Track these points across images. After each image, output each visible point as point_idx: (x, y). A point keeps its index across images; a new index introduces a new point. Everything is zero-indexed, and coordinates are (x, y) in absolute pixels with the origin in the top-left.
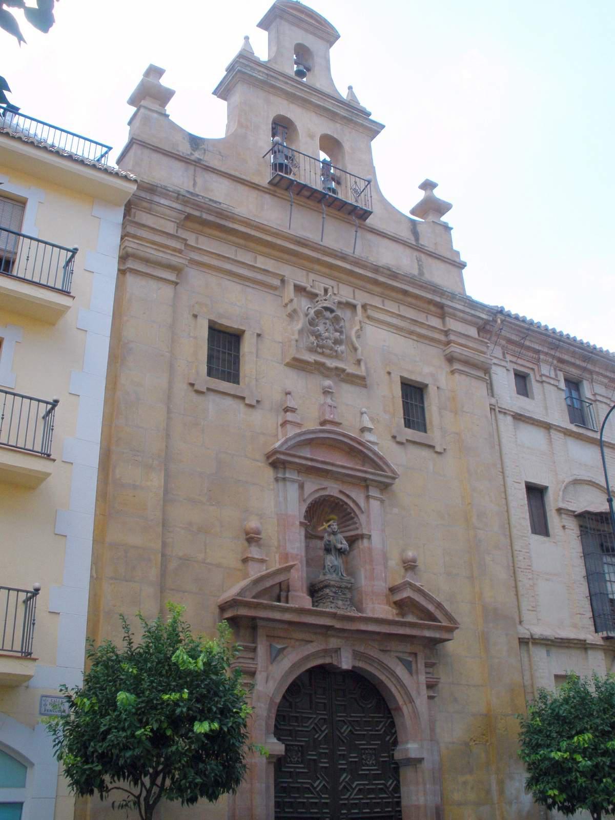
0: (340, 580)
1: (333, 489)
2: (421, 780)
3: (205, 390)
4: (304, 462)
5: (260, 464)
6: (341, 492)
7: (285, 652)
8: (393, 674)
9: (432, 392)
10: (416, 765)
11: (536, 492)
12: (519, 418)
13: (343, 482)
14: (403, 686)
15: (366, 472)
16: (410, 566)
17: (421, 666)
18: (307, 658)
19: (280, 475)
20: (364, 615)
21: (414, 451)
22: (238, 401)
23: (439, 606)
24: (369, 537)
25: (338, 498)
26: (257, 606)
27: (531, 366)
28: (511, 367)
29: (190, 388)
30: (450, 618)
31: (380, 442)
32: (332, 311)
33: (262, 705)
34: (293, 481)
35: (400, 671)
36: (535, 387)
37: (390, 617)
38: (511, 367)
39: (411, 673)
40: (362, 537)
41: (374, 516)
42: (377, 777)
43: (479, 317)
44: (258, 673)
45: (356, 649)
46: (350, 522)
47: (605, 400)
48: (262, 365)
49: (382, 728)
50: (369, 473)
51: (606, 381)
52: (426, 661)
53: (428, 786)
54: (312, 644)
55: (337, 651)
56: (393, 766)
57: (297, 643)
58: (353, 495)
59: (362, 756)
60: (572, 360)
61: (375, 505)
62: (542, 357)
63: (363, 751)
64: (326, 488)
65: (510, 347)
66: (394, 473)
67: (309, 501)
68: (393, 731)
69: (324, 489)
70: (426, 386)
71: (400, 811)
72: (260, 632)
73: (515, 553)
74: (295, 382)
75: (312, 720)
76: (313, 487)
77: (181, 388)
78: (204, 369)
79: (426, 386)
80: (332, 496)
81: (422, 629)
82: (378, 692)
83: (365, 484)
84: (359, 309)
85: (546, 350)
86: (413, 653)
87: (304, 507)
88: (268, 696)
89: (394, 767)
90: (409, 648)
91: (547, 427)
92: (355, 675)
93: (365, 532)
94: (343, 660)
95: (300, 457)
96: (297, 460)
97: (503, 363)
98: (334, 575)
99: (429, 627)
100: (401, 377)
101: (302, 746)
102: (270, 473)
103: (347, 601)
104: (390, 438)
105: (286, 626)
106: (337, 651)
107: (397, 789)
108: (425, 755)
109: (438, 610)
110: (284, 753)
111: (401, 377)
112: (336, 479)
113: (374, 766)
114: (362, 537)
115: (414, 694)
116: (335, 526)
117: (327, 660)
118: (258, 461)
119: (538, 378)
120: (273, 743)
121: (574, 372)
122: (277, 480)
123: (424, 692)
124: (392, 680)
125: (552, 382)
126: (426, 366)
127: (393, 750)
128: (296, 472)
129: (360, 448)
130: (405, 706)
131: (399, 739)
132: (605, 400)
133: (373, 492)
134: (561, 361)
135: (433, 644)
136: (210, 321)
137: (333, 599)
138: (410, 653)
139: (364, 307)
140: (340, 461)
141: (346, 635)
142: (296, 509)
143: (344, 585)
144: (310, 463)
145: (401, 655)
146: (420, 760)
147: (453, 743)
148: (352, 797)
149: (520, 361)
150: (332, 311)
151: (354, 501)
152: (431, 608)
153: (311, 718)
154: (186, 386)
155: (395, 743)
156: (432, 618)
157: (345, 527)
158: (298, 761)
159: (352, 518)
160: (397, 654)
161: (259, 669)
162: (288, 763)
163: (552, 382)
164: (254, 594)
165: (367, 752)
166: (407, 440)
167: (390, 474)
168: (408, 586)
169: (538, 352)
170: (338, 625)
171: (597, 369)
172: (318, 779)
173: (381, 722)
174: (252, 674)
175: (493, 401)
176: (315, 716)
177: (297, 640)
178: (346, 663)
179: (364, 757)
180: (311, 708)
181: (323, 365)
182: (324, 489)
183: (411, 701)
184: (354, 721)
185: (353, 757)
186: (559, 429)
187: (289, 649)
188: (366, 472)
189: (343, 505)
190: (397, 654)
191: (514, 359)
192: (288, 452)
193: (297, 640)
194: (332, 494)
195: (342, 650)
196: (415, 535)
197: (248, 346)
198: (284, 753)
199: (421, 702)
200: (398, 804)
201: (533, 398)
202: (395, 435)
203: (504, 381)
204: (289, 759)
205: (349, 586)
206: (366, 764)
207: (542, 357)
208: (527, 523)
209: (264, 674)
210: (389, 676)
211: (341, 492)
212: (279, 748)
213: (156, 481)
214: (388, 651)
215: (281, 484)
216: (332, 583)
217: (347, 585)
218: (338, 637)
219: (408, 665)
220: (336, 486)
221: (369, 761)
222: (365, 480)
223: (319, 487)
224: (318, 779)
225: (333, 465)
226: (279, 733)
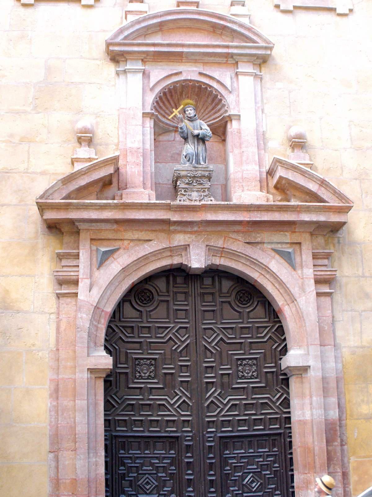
0: (193, 169)
1: (190, 72)
2: (307, 392)
4: (152, 49)
5: (98, 62)
6: (201, 74)
7: (115, 256)
8: (266, 269)
10: (301, 374)
13: (205, 63)
14: (281, 283)
15: (228, 47)
16: (298, 143)
17: (306, 256)
18: (145, 259)
19: (121, 69)
20: (231, 203)
23: (323, 183)
24: (238, 117)
25: (198, 82)
26: (67, 207)
30: (340, 196)
33: (84, 316)
34: (135, 71)
35: (276, 265)
37: (262, 202)
39: (293, 266)
40: (230, 118)
41: (241, 93)
42: (260, 390)
44: (80, 280)
45: (212, 244)
46: (219, 106)
49: (265, 335)
50: (235, 47)
52: (314, 251)
53: (314, 398)
54: (151, 243)
55: (186, 247)
56: (281, 377)
57: (132, 244)
58: (216, 75)
59: (238, 367)
61: (246, 83)
63: (239, 362)
64: (181, 73)
66: (267, 43)
67: (158, 89)
68: (283, 338)
69: (176, 74)
71: (290, 428)
72: (82, 235)
75: (169, 329)
76: (159, 73)
80: (190, 81)
82: (261, 293)
83: (230, 60)
86: (297, 243)
87: (151, 98)
88: (92, 305)
89: (283, 379)
90: (287, 237)
92: (214, 273)
93: (232, 112)
94: (193, 257)
96: (136, 49)
98: (188, 164)
99: (308, 210)
101: (155, 359)
102: (111, 68)
103: (204, 191)
104: (272, 7)
105: (115, 226)
106: (186, 247)
107: (286, 403)
108: (311, 363)
109: (323, 189)
110: (111, 367)
112: (196, 62)
113: (256, 378)
114: (230, 118)
115: (295, 291)
116: (189, 111)
117: (176, 261)
118: (97, 59)
120: (101, 356)
122: (118, 74)
123: (311, 287)
124: (267, 276)
127: (281, 359)
128: (140, 61)
129: (222, 22)
130: (287, 307)
131: (288, 347)
135: (335, 229)
137: (185, 191)
138: (292, 243)
141: (196, 229)
143: (199, 173)
144: (152, 49)
145: (279, 247)
146: (305, 369)
147: (363, 347)
148: (223, 413)
151: (218, 82)
152: (313, 187)
153: (167, 328)
155: (285, 351)
156: (315, 197)
157: (216, 113)
158: (149, 376)
159: (221, 100)
160: (273, 246)
161: (81, 276)
162: (138, 379)
164: (64, 195)
165: (244, 362)
166: (295, 7)
168: (278, 164)
170: (175, 217)
172: (177, 395)
173: (266, 327)
174: (76, 283)
176: (172, 325)
177: (132, 240)
178: (197, 261)
179: (240, 368)
180: (168, 317)
182: (176, 74)
183: (293, 300)
184: (224, 328)
185: (226, 369)
187: (121, 251)
188: (228, 47)
189: (206, 88)
190: (273, 246)
192: (126, 41)
193: (132, 240)
194: (189, 78)
195: (191, 247)
198: (111, 367)
200: (288, 420)
202: (278, 3)
204: (138, 374)
205: (207, 174)
206: (243, 376)
209: (88, 281)
210: (263, 273)
211: (201, 74)
214: (258, 243)
215: (122, 77)
216: (183, 173)
217: (203, 173)
218: (185, 232)
219: (287, 257)
220: (195, 69)
221: (248, 373)
222: (232, 55)
223: (170, 73)
224: (177, 395)
225: (183, 46)
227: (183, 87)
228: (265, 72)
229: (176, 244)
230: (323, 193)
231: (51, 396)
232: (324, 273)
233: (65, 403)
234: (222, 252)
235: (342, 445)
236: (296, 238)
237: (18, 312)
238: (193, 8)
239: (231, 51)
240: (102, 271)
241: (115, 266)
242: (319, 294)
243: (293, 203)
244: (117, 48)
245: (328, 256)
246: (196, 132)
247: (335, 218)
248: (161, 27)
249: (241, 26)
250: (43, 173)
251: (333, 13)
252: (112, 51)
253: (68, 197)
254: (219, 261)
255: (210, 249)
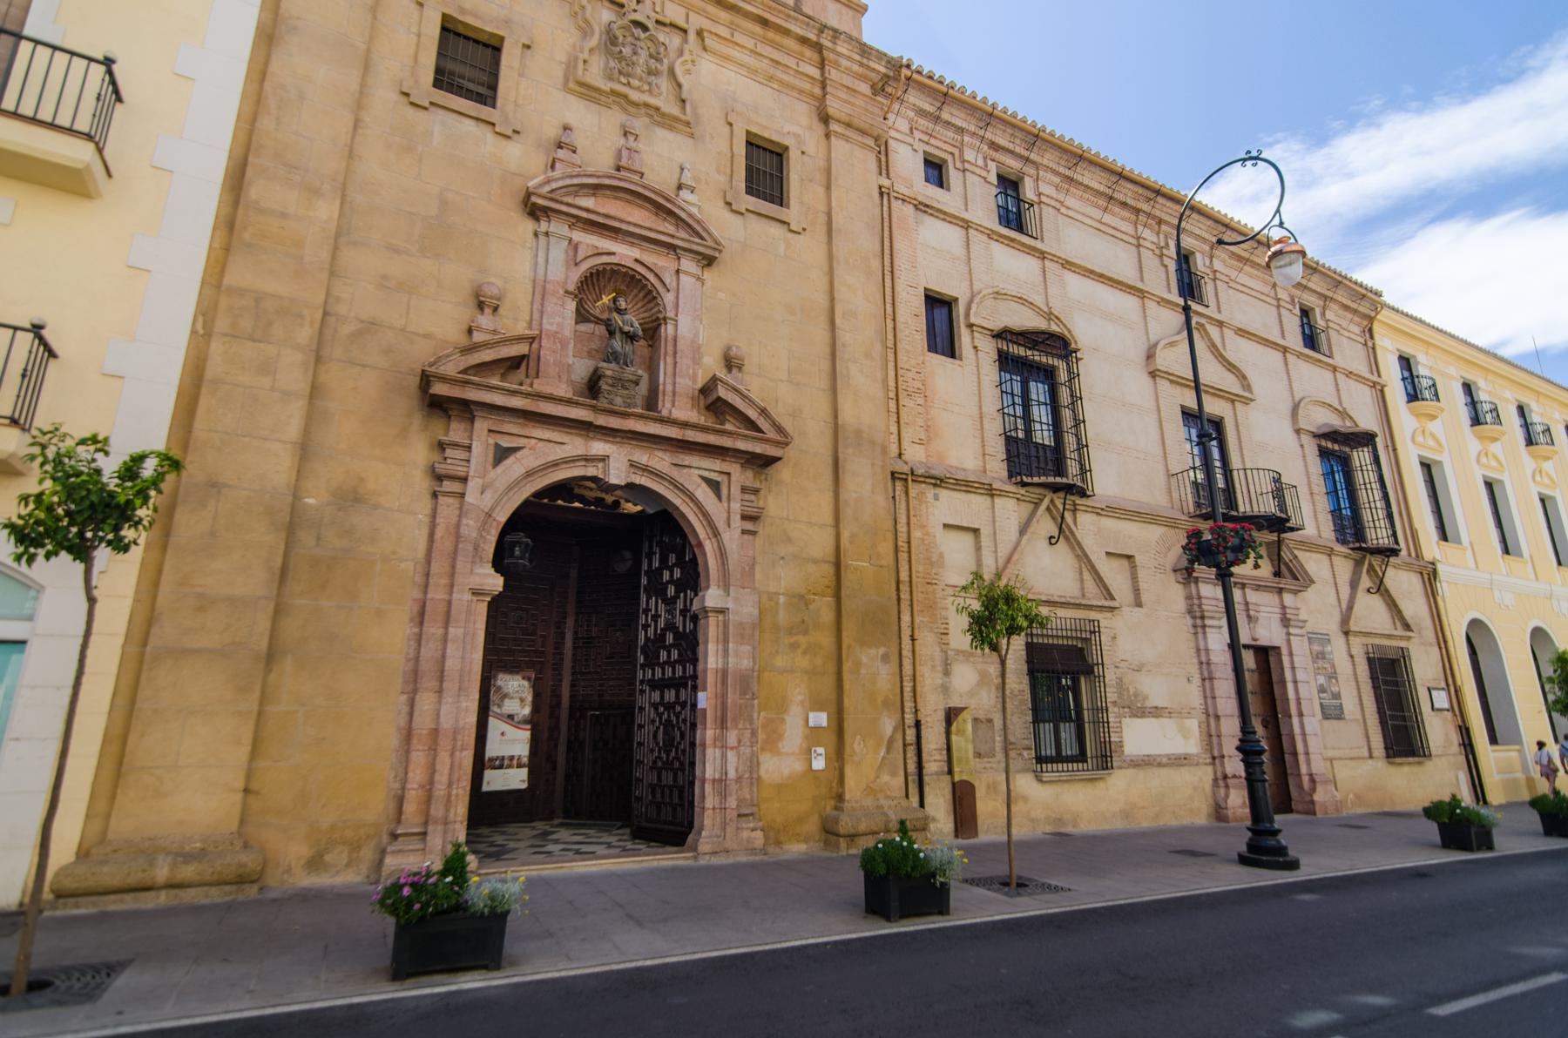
1: (625, 253)
3: (426, 104)
9: (794, 156)
11: (937, 304)
12: (923, 207)
21: (756, 225)
22: (483, 127)
23: (763, 412)
27: (950, 149)
28: (921, 147)
29: (404, 99)
30: (779, 429)
31: (702, 204)
32: (645, 28)
34: (561, 237)
36: (953, 176)
38: (921, 147)
43: (874, 70)
47: (1053, 203)
48: (532, 87)
50: (681, 237)
51: (1057, 180)
60: (1011, 146)
62: (966, 139)
65: (922, 122)
67: (584, 267)
70: (786, 148)
73: (900, 372)
74: (579, 114)
77: (384, 97)
78: (428, 75)
79: (786, 148)
81: (737, 433)
84: (692, 36)
85: (972, 128)
87: (576, 275)
91: (966, 225)
95: (568, 205)
97: (910, 140)
100: (748, 132)
111: (748, 132)
115: (721, 525)
117: (591, 471)
119: (959, 165)
121: (1013, 164)
123: (737, 522)
125: (978, 171)
126: (789, 123)
132: (1053, 203)
133: (688, 264)
134: (994, 146)
136: (444, 15)
139: (700, 33)
140: (637, 217)
142: (561, 272)
145: (706, 474)
149: (933, 141)
150: (645, 28)
152: (752, 414)
154: (396, 97)
163: (978, 171)
167: (710, 243)
169: (961, 130)
171: (1045, 162)
175: (886, 183)
181: (625, 97)
186: (980, 229)
191: (926, 138)
196: (742, 313)
197: (509, 59)
199: (732, 537)
201: (949, 190)
203: (908, 163)
207: (966, 139)
208: (921, 338)
212: (496, 583)
213: (326, 211)
225: (622, 221)
226: (498, 564)
227: (613, 271)
228: (707, 275)
229: (593, 452)
230: (762, 423)
231: (411, 620)
232: (751, 511)
233: (432, 630)
234: (645, 469)
235: (1076, 426)
236: (726, 467)
237: (376, 507)
238: (636, 178)
239: (676, 242)
240: (500, 469)
241: (514, 467)
242: (744, 532)
243: (728, 427)
244: (540, 201)
245: (756, 491)
246: (626, 328)
247: (771, 451)
248: (596, 189)
249: (690, 215)
250: (427, 336)
251: (489, 128)
252: (534, 204)
253: (465, 371)
254: (639, 479)
255: (633, 465)
